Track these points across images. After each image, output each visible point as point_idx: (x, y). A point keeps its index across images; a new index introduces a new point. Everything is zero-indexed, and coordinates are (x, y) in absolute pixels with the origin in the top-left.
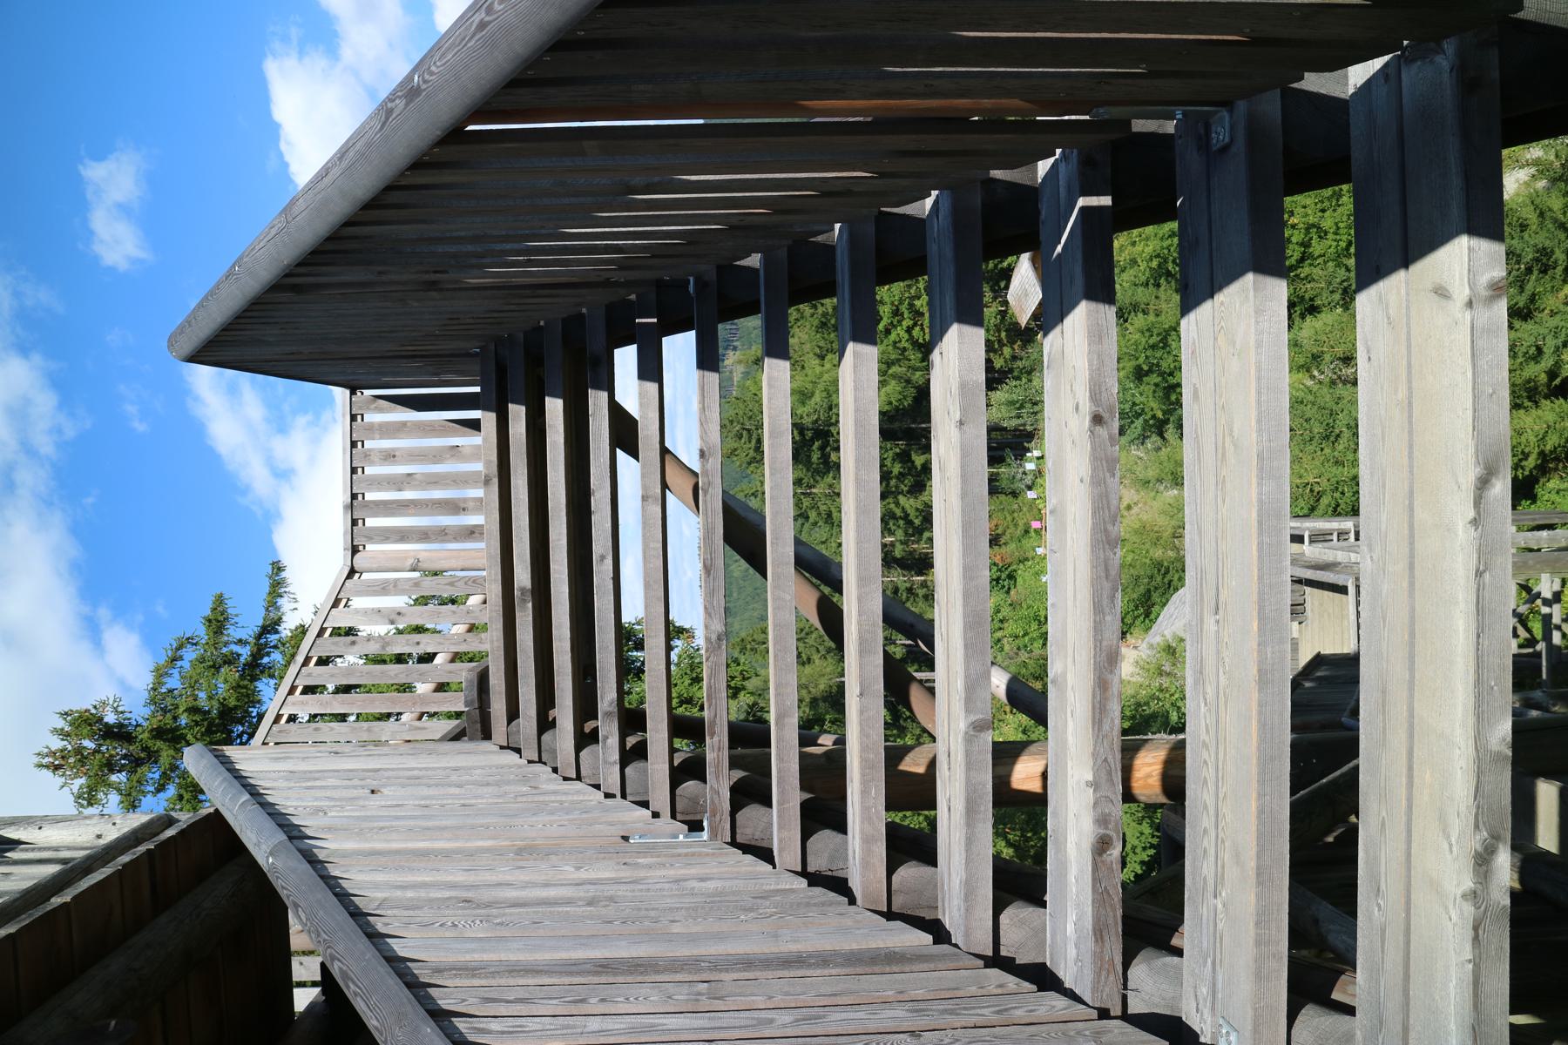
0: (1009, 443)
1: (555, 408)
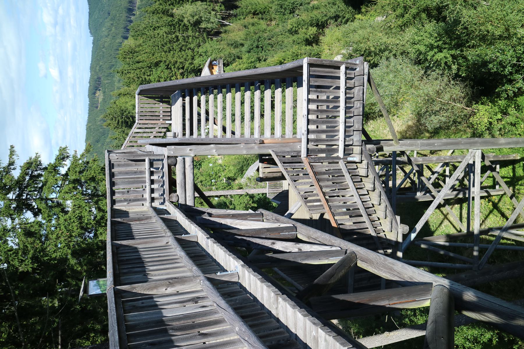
0: (242, 103)
1: (187, 99)
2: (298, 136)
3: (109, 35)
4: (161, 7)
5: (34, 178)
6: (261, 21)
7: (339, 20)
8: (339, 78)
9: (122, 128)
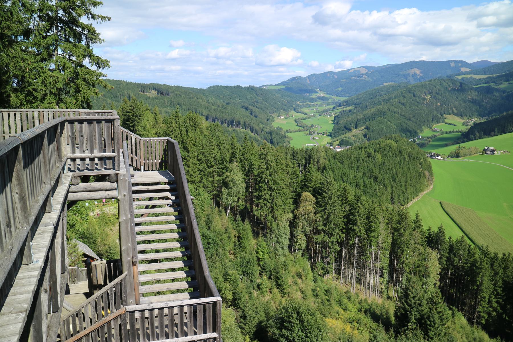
1: (167, 187)
2: (142, 299)
3: (209, 103)
4: (238, 151)
5: (78, 37)
6: (233, 245)
7: (242, 320)
8: (205, 332)
9: (123, 115)
